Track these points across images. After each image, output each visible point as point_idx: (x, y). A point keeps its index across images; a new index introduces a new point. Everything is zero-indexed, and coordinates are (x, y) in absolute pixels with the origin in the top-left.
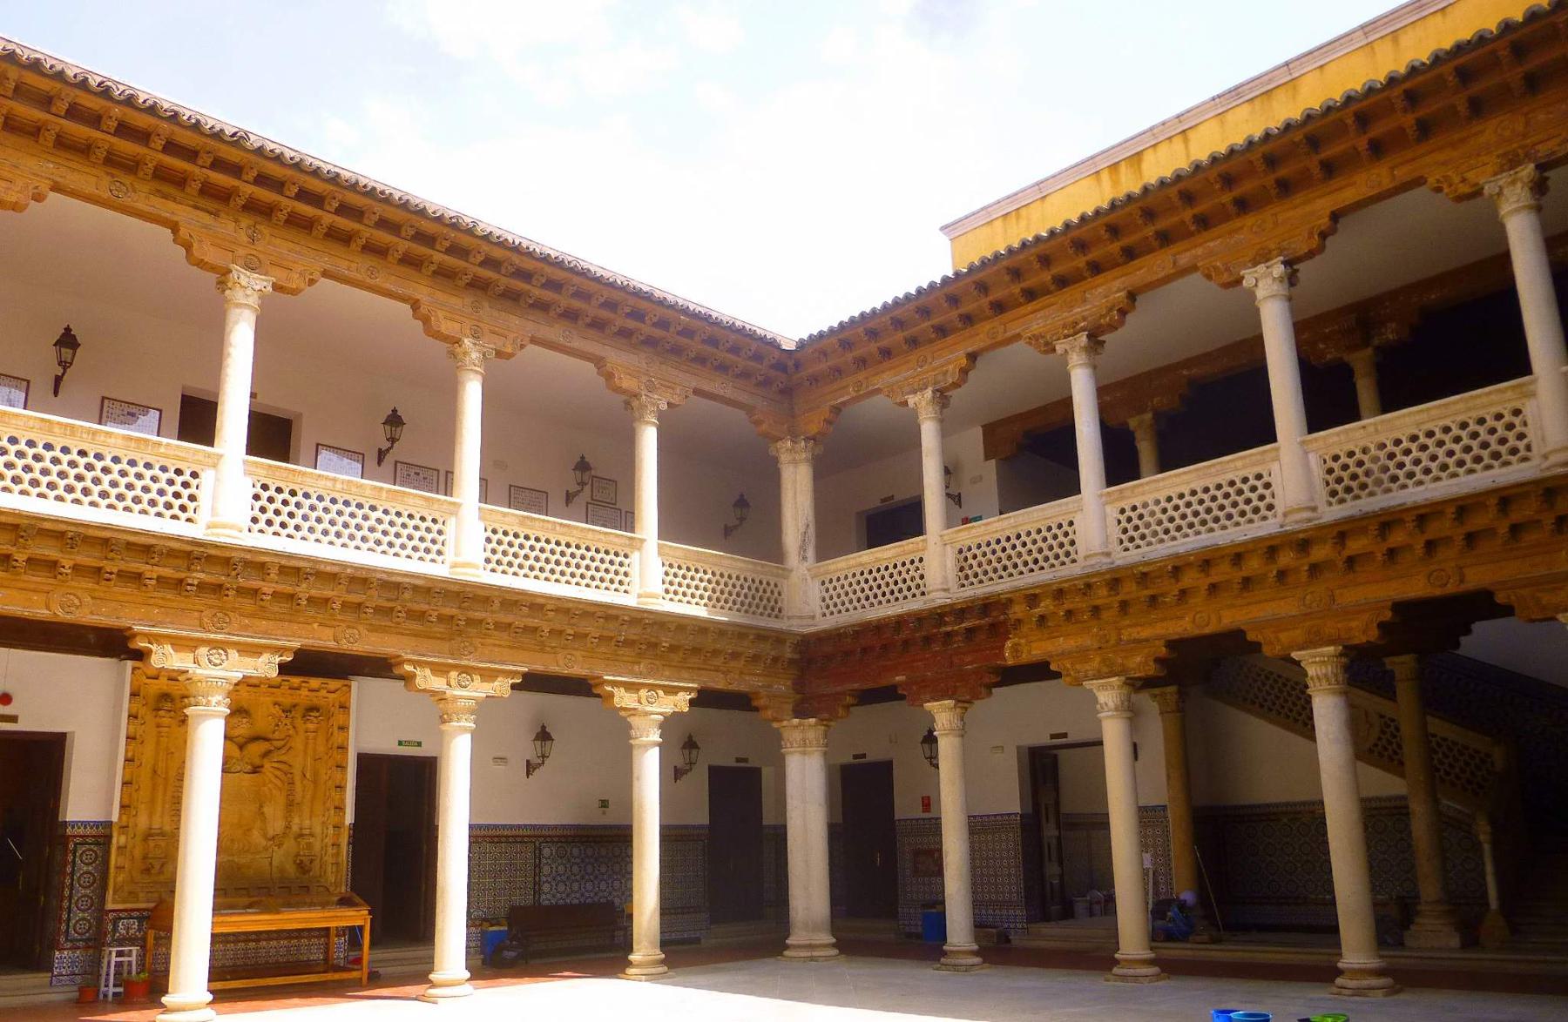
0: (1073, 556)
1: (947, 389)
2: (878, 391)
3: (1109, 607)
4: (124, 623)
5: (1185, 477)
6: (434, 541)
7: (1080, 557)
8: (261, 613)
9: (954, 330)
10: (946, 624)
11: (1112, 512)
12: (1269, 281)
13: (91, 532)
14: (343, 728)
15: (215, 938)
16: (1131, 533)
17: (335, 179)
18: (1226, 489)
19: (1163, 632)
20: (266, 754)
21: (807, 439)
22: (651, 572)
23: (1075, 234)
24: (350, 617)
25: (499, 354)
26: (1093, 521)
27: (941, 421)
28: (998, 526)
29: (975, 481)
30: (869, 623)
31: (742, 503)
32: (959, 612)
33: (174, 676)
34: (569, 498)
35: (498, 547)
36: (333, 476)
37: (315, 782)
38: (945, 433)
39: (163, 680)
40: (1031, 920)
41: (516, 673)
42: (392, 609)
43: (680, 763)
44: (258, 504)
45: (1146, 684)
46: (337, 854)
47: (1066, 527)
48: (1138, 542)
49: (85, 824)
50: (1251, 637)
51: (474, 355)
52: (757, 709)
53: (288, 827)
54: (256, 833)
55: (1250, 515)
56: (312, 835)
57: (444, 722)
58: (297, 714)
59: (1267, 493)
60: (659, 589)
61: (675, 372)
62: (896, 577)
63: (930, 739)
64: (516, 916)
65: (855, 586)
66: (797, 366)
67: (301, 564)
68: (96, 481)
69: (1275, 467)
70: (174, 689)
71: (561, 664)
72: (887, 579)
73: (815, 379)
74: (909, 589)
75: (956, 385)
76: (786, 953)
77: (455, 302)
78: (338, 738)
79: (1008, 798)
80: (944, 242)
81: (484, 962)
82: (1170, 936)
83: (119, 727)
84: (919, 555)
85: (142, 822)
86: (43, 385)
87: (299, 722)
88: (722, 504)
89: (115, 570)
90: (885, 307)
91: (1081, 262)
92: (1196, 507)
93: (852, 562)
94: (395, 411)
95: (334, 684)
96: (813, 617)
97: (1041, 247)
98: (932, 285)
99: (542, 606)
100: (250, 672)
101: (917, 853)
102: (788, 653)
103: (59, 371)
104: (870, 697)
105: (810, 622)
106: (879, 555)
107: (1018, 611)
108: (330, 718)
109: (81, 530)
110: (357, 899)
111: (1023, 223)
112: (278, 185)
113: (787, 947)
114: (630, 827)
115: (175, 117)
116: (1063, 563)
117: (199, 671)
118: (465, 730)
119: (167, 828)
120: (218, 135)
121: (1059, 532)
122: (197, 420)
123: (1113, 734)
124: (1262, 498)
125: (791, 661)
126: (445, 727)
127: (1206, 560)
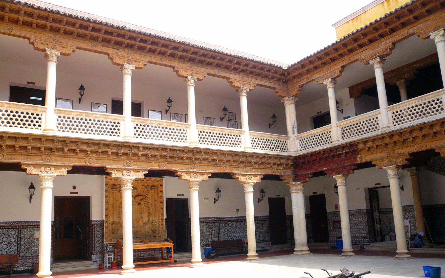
0: (378, 128)
1: (336, 78)
2: (314, 80)
3: (390, 143)
4: (104, 165)
5: (413, 101)
6: (184, 136)
7: (380, 128)
8: (139, 160)
9: (337, 59)
10: (339, 151)
11: (390, 114)
12: (439, 36)
13: (94, 142)
14: (162, 191)
15: (134, 251)
16: (396, 120)
17: (150, 35)
18: (427, 104)
19: (408, 151)
20: (142, 200)
21: (293, 96)
22: (247, 140)
23: (374, 26)
24: (162, 160)
25: (199, 79)
26: (385, 117)
27: (334, 88)
28: (356, 119)
29: (347, 105)
30: (315, 152)
31: (274, 117)
32: (343, 147)
33: (117, 179)
34: (222, 119)
35: (202, 136)
36: (154, 118)
37: (155, 207)
38: (336, 91)
39: (113, 180)
40: (371, 242)
41: (210, 173)
42: (174, 157)
43: (260, 197)
44: (135, 130)
45: (404, 167)
46: (163, 227)
47: (375, 119)
48: (399, 122)
49: (97, 221)
50: (437, 151)
51: (192, 81)
52: (282, 180)
53: (149, 220)
54: (140, 222)
55: (435, 112)
56: (155, 222)
57: (190, 188)
58: (149, 188)
59: (441, 105)
60: (250, 145)
61: (251, 79)
62: (323, 137)
63: (336, 187)
64: (214, 244)
65: (310, 141)
66: (288, 74)
67: (148, 146)
68: (94, 127)
69: (443, 96)
70: (117, 183)
71: (223, 170)
72: (320, 138)
73: (294, 77)
74: (327, 141)
75: (338, 76)
76: (294, 253)
77: (185, 66)
78: (160, 195)
79: (362, 204)
80: (333, 29)
81: (205, 257)
82: (416, 246)
83: (103, 193)
84: (329, 130)
85: (111, 219)
86: (76, 101)
87: (149, 190)
88: (269, 118)
89: (101, 151)
90: (314, 54)
91: (376, 35)
92: (417, 110)
93: (309, 134)
94: (169, 98)
95: (158, 179)
96: (298, 151)
97: (363, 31)
98: (329, 46)
99: (216, 153)
100: (137, 177)
101: (334, 222)
102: (290, 162)
103: (80, 97)
104: (315, 175)
105: (297, 152)
106: (317, 131)
107: (361, 146)
108: (158, 188)
109: (92, 141)
110: (169, 239)
111: (359, 21)
112: (134, 39)
113: (294, 251)
114: (246, 217)
115: (107, 24)
116: (375, 131)
117: (124, 178)
118: (196, 190)
119: (117, 221)
120: (118, 28)
121: (373, 121)
122: (117, 107)
123: (394, 184)
124: (439, 106)
125: (291, 165)
126: (190, 190)
127: (421, 127)
